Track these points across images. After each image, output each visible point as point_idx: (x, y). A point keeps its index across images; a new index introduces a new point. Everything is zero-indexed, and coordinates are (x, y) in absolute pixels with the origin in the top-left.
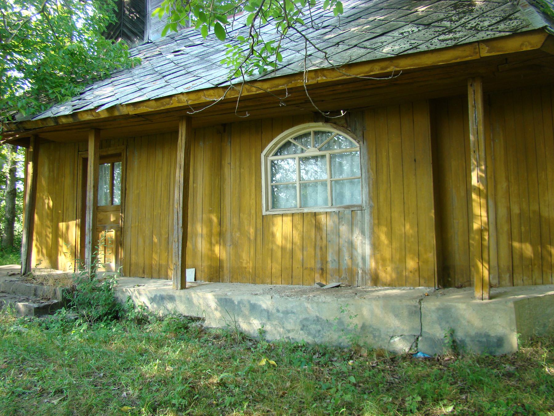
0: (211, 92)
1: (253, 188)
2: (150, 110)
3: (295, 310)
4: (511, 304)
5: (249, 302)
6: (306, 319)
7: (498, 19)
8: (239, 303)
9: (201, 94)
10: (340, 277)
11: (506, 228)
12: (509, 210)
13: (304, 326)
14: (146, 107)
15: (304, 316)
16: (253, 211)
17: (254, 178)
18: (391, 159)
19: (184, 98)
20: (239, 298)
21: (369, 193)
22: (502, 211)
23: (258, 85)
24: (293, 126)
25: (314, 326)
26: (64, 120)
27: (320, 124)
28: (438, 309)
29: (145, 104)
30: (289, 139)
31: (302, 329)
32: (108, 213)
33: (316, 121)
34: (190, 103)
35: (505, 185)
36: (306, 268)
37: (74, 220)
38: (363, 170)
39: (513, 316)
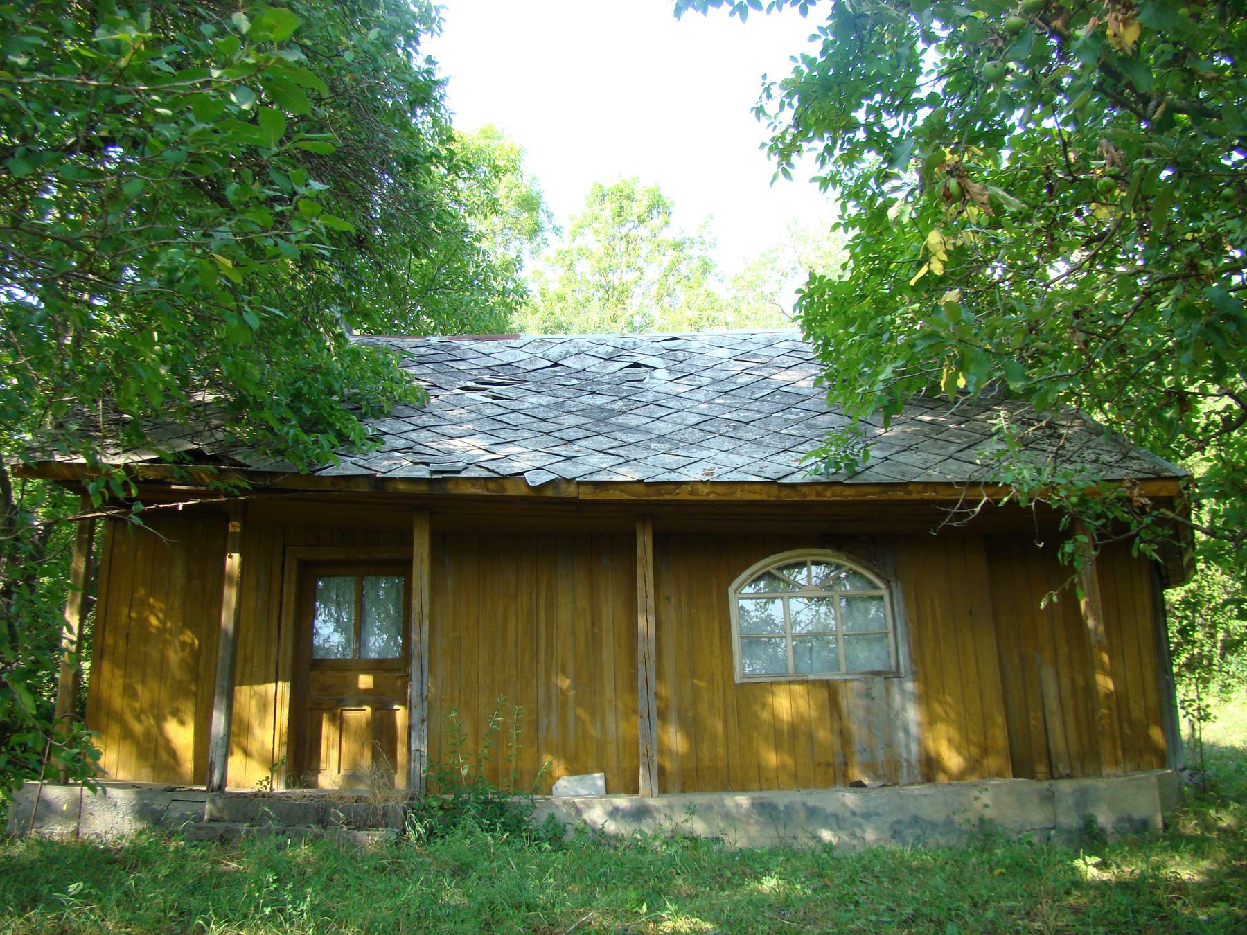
0: (758, 487)
1: (716, 639)
2: (626, 497)
3: (880, 811)
4: (1154, 779)
5: (805, 804)
6: (899, 822)
7: (896, 449)
8: (787, 807)
9: (739, 487)
10: (875, 773)
11: (1071, 704)
12: (1073, 680)
13: (895, 832)
14: (622, 491)
15: (895, 818)
16: (718, 678)
17: (716, 625)
18: (938, 611)
19: (704, 490)
20: (787, 800)
21: (910, 654)
22: (1066, 682)
23: (838, 489)
24: (782, 550)
25: (911, 831)
26: (402, 487)
27: (829, 551)
28: (1075, 791)
29: (622, 487)
30: (770, 568)
31: (893, 837)
32: (348, 674)
33: (822, 546)
34: (712, 497)
35: (1066, 650)
36: (819, 764)
37: (270, 682)
38: (898, 623)
39: (1157, 793)
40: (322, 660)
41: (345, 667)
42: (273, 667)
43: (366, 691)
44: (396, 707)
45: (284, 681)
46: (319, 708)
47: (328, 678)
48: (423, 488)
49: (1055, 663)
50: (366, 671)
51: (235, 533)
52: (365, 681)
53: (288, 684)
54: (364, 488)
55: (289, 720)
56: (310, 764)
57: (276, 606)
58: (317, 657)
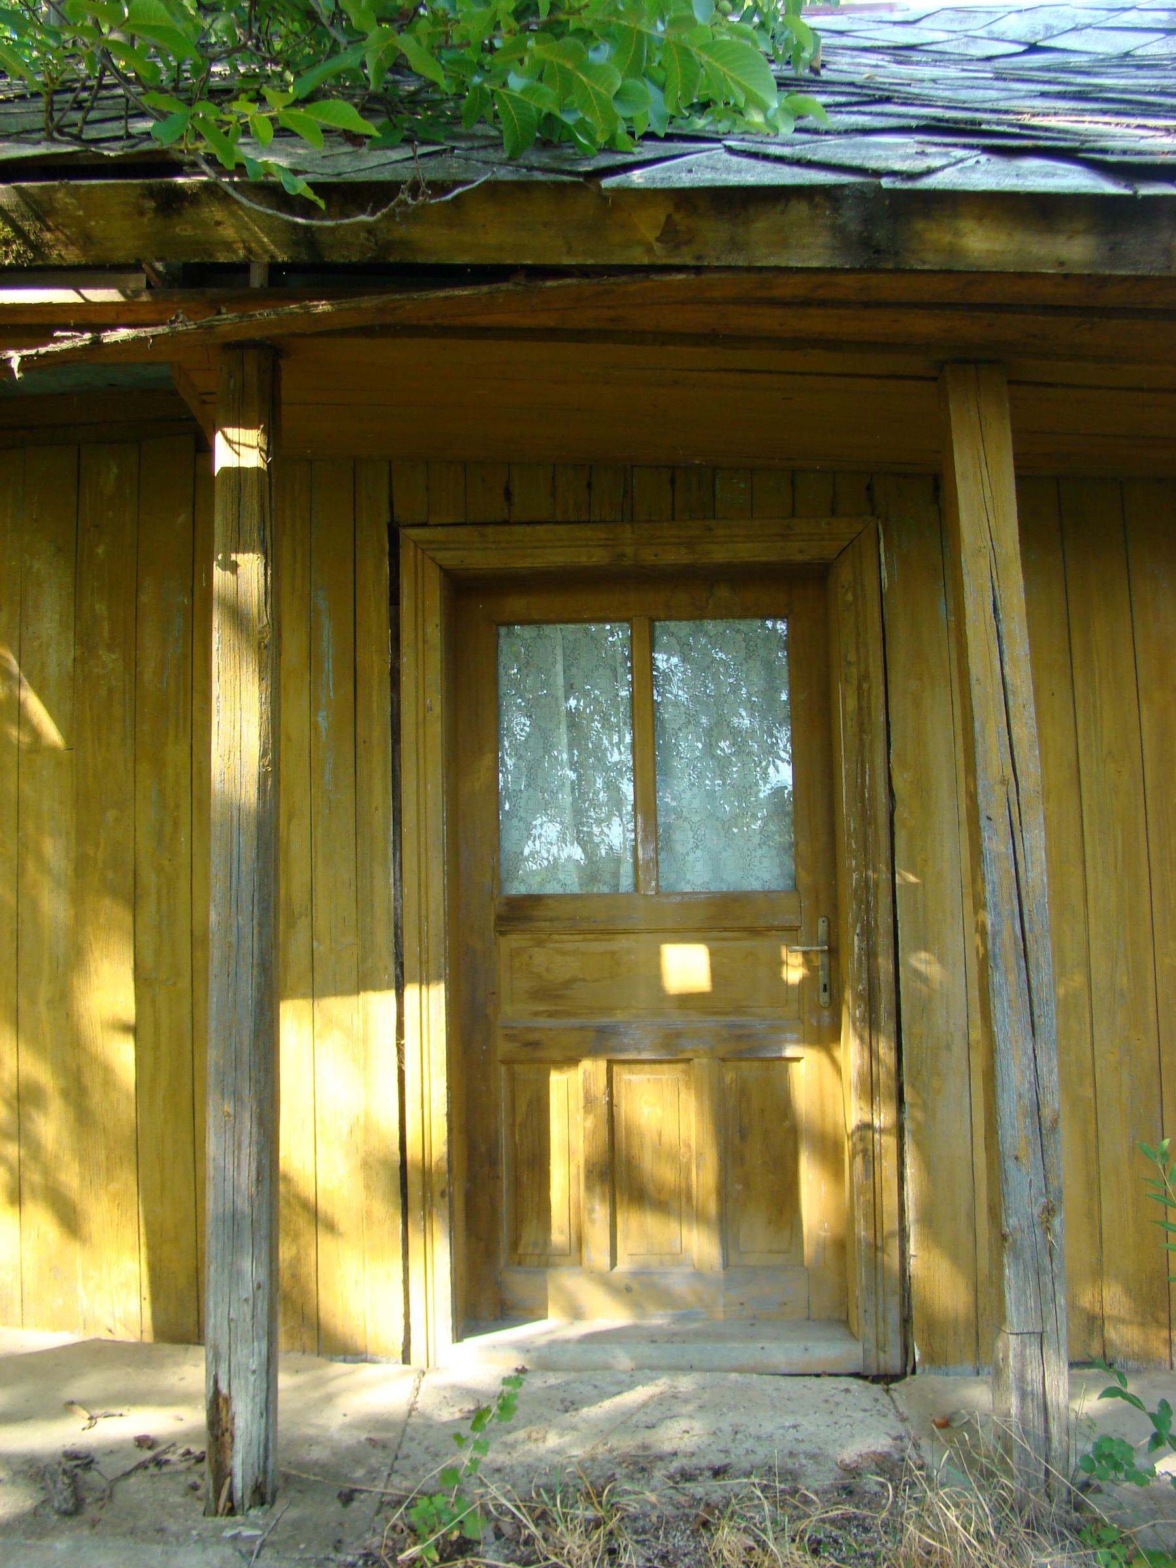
32: (622, 943)
40: (535, 900)
41: (612, 919)
42: (383, 938)
43: (687, 1000)
44: (790, 1051)
45: (424, 980)
46: (541, 1054)
47: (558, 958)
48: (1075, 250)
49: (177, 727)
50: (684, 934)
51: (237, 474)
52: (686, 967)
53: (437, 994)
54: (811, 249)
55: (449, 1115)
56: (515, 1245)
57: (379, 733)
58: (517, 888)
